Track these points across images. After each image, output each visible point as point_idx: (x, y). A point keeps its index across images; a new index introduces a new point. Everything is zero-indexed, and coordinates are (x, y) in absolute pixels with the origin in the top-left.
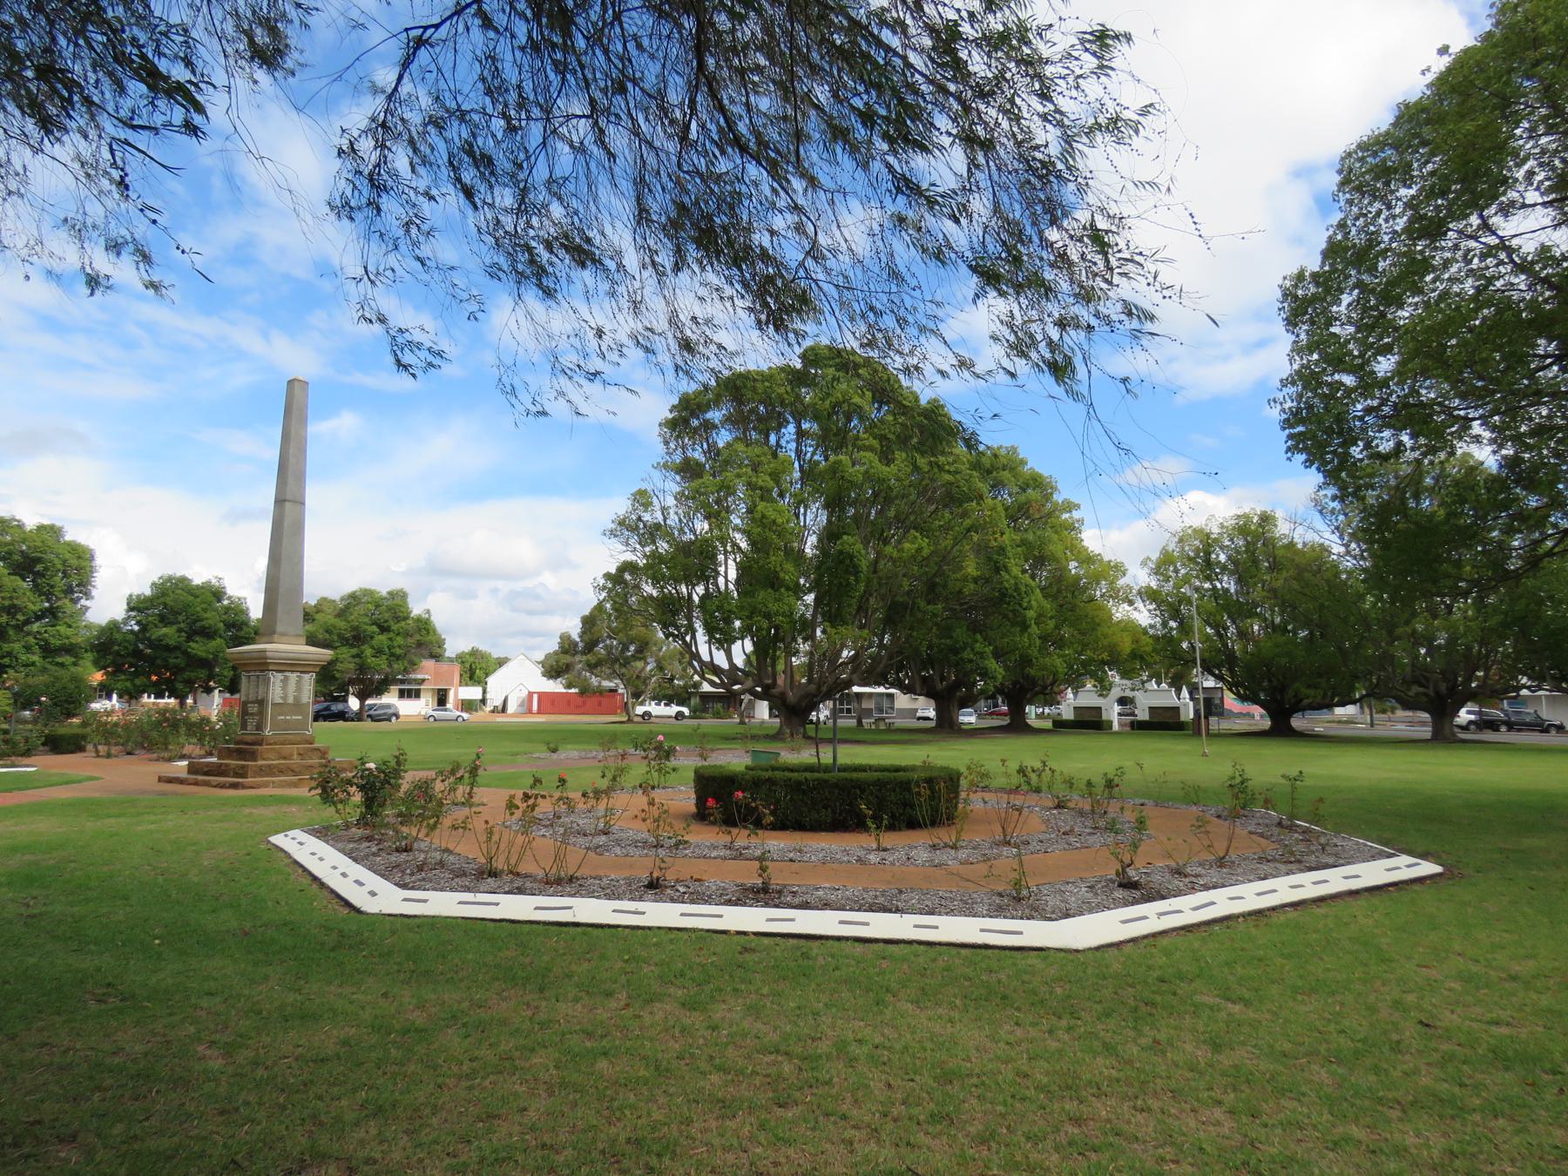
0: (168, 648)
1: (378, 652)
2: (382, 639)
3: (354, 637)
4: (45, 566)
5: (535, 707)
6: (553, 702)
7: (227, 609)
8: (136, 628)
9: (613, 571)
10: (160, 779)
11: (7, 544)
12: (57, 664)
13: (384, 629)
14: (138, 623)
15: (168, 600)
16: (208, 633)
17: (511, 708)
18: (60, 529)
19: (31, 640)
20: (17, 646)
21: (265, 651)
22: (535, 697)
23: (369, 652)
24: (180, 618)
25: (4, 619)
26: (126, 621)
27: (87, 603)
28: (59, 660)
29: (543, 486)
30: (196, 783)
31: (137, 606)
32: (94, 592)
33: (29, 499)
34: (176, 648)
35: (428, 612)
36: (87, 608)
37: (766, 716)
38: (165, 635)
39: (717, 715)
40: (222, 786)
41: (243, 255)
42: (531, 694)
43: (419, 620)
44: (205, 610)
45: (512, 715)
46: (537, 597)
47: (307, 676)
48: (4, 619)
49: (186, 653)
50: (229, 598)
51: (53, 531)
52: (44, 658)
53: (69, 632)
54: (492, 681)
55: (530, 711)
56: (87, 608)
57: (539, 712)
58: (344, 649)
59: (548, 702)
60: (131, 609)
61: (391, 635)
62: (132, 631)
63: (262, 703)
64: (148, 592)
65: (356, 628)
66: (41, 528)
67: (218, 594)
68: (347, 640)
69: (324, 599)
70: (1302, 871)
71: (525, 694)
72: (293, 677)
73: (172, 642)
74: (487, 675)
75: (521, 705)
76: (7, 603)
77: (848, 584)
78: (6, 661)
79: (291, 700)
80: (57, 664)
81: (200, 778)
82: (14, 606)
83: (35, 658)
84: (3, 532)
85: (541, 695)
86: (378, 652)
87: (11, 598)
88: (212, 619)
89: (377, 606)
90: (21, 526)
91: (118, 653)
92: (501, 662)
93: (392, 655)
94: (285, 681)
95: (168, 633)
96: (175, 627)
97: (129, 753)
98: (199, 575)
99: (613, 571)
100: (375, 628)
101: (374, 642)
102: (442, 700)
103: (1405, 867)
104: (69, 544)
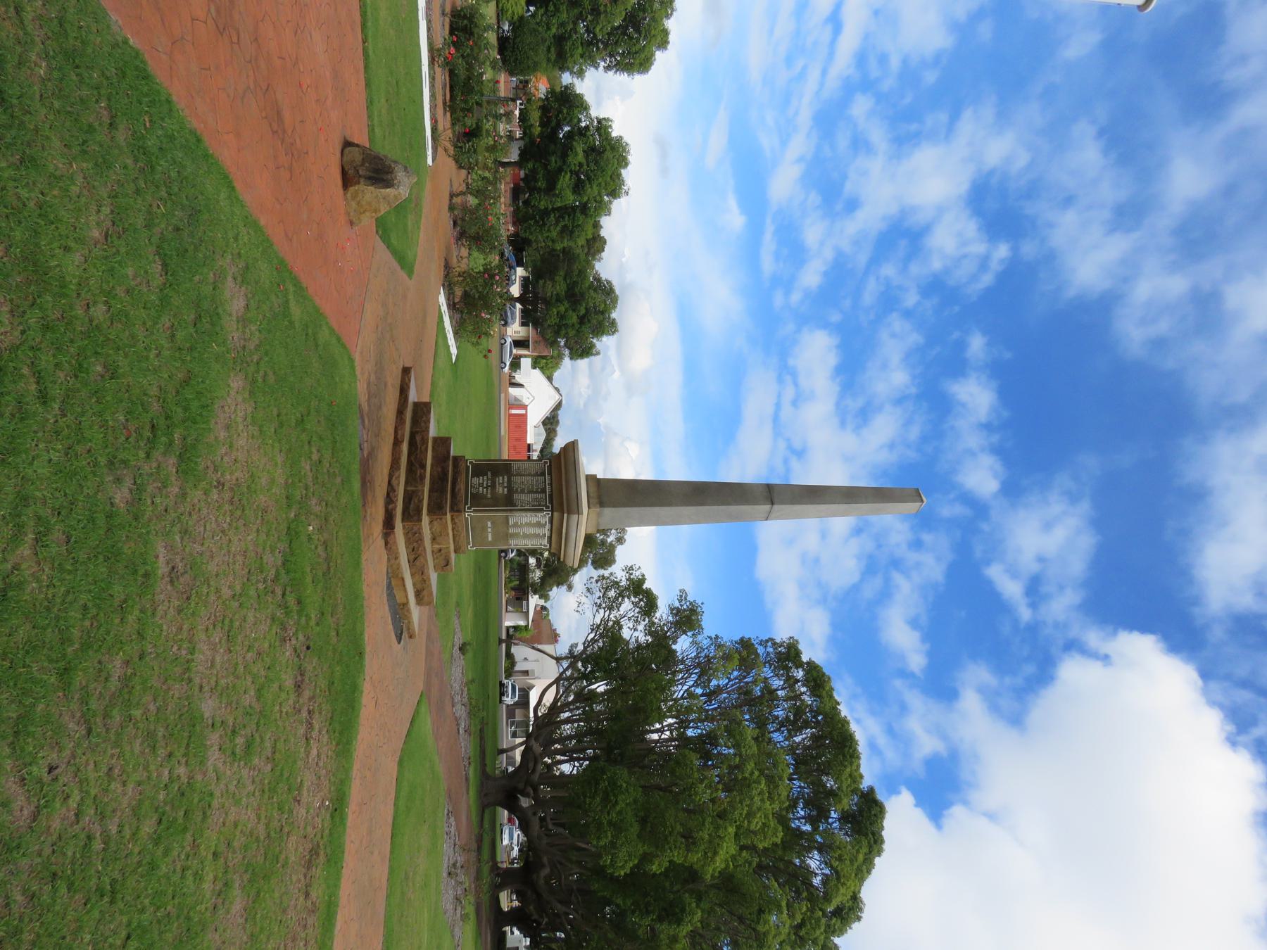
0: (564, 156)
1: (562, 317)
2: (573, 318)
4: (633, 38)
5: (514, 412)
7: (601, 201)
8: (583, 124)
10: (406, 371)
11: (652, 7)
12: (549, 48)
13: (582, 320)
14: (587, 127)
15: (608, 154)
16: (578, 187)
17: (513, 391)
18: (665, 48)
19: (570, 26)
20: (564, 16)
21: (579, 512)
22: (523, 412)
24: (592, 166)
25: (587, 4)
26: (589, 117)
27: (601, 68)
28: (553, 49)
30: (400, 412)
31: (602, 126)
32: (611, 73)
33: (685, 22)
34: (564, 162)
35: (598, 353)
36: (597, 68)
37: (507, 624)
38: (576, 155)
39: (509, 580)
41: (860, 144)
43: (592, 346)
44: (599, 185)
45: (507, 393)
46: (603, 369)
47: (545, 541)
48: (587, 4)
49: (560, 170)
50: (610, 202)
51: (663, 44)
52: (554, 36)
53: (577, 56)
55: (512, 407)
56: (597, 68)
60: (599, 121)
61: (577, 326)
62: (580, 121)
64: (614, 134)
65: (582, 295)
66: (666, 33)
67: (615, 193)
69: (605, 242)
71: (526, 402)
72: (546, 531)
73: (570, 159)
74: (542, 369)
75: (516, 399)
76: (602, 9)
77: (648, 912)
78: (551, 8)
80: (549, 48)
82: (599, 14)
83: (554, 30)
84: (662, 3)
85: (524, 417)
86: (562, 317)
87: (605, 11)
88: (591, 191)
90: (668, 16)
91: (560, 112)
92: (550, 379)
94: (539, 525)
95: (578, 155)
96: (584, 161)
97: (455, 223)
98: (631, 175)
100: (583, 311)
102: (519, 344)
103: (454, 351)
104: (653, 55)
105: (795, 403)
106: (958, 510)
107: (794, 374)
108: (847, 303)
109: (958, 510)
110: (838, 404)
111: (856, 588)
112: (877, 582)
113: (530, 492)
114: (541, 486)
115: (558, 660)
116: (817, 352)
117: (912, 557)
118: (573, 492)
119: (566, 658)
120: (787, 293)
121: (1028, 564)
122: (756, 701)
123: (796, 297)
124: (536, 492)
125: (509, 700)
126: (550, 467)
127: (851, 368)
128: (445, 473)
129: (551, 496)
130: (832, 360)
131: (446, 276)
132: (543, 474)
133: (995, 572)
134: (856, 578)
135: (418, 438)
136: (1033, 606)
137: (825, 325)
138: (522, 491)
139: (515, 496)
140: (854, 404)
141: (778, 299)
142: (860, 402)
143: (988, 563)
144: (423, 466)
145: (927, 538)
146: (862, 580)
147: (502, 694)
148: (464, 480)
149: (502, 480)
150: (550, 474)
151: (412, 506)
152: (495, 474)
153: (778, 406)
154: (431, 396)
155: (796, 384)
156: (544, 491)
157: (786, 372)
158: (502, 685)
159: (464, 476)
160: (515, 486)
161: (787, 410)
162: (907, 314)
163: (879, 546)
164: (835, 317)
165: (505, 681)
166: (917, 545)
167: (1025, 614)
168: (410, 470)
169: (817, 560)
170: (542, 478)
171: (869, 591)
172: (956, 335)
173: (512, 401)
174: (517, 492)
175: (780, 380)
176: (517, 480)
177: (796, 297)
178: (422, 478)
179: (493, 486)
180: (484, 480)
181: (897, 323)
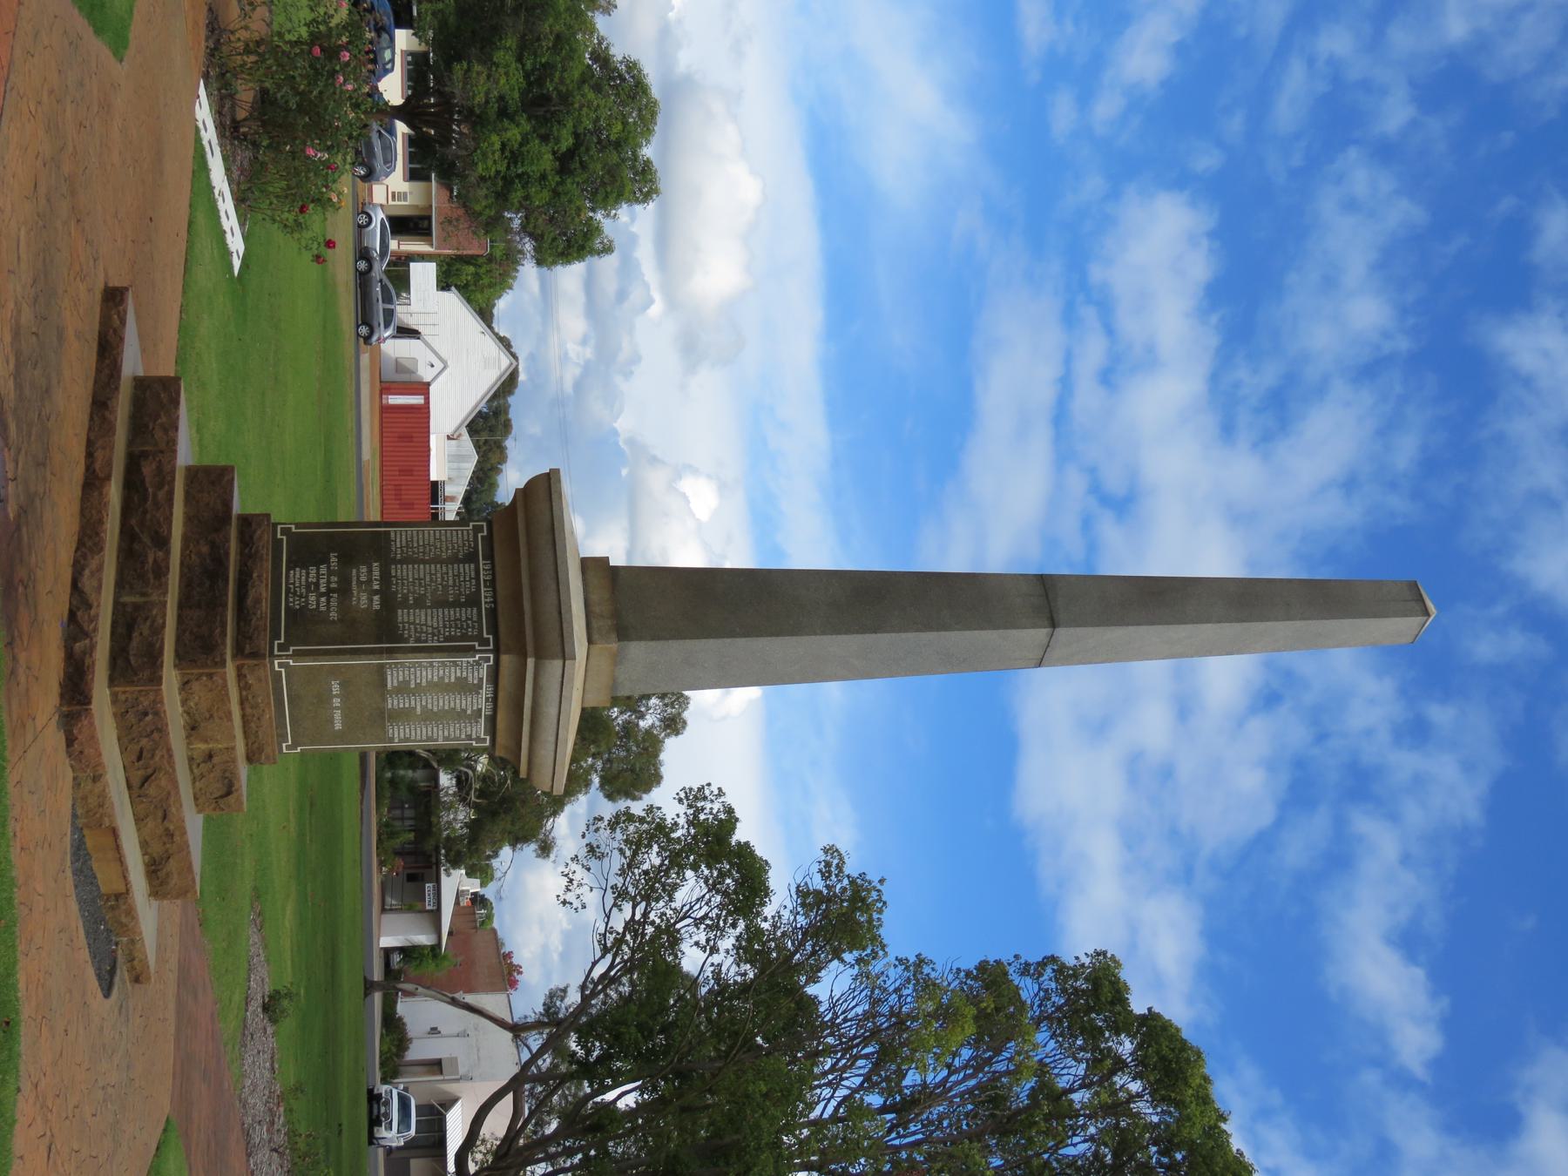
3: (544, 100)
6: (406, 438)
9: (740, 835)
10: (113, 297)
13: (565, 162)
22: (417, 400)
23: (514, 134)
29: (845, 291)
30: (100, 404)
37: (386, 941)
40: (93, 482)
42: (423, 388)
43: (592, 230)
47: (481, 728)
54: (452, 299)
55: (387, 388)
57: (386, 410)
58: (517, 78)
59: (407, 430)
61: (554, 179)
63: (384, 633)
65: (565, 98)
68: (540, 82)
70: (178, 793)
71: (425, 374)
72: (482, 701)
75: (399, 366)
79: (393, 703)
81: (114, 493)
85: (423, 412)
89: (618, 145)
93: (508, 182)
94: (463, 687)
99: (740, 835)
100: (567, 142)
101: (535, 143)
102: (402, 225)
105: (1108, 377)
106: (1517, 644)
107: (1105, 306)
108: (1235, 125)
109: (1517, 644)
110: (1214, 378)
111: (1264, 841)
113: (441, 603)
114: (468, 589)
115: (518, 1030)
116: (1161, 249)
117: (1405, 762)
120: (1085, 99)
123: (1106, 108)
124: (456, 604)
125: (392, 1136)
126: (489, 540)
127: (1244, 294)
128: (219, 561)
129: (493, 613)
130: (1200, 268)
131: (212, 53)
132: (471, 557)
134: (1266, 816)
137: (1181, 181)
138: (419, 603)
139: (402, 615)
140: (1256, 380)
141: (1063, 114)
142: (1270, 375)
144: (162, 542)
145: (1441, 715)
146: (1279, 823)
147: (374, 1122)
149: (366, 573)
150: (490, 556)
153: (1066, 384)
155: (1110, 331)
156: (473, 601)
157: (1083, 298)
158: (374, 1098)
159: (269, 565)
160: (400, 590)
161: (1087, 396)
162: (1384, 152)
163: (1321, 738)
164: (1206, 160)
165: (383, 1089)
166: (1416, 732)
169: (1167, 773)
170: (469, 568)
171: (1297, 850)
172: (1507, 204)
173: (390, 375)
174: (404, 604)
175: (1069, 318)
177: (1106, 108)
178: (161, 571)
179: (344, 590)
180: (322, 576)
181: (1360, 175)
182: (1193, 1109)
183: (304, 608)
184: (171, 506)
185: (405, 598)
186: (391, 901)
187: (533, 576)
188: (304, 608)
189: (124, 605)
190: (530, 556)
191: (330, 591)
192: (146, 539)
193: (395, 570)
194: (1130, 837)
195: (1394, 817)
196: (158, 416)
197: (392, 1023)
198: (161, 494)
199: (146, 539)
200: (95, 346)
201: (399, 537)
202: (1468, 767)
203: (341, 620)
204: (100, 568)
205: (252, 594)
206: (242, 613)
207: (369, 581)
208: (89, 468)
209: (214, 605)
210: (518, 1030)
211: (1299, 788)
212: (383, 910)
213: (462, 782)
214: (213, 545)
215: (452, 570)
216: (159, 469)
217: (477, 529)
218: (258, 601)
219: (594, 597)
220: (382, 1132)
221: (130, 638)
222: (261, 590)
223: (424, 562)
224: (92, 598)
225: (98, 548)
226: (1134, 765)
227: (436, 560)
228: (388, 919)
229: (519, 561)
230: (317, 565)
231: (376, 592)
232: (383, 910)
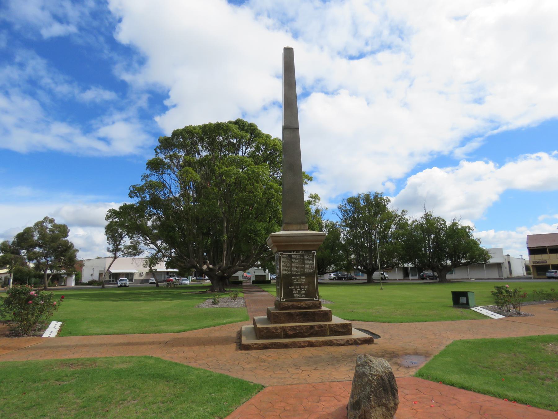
9: (117, 209)
37: (73, 285)
111: (43, 105)
112: (40, 92)
113: (303, 262)
114: (299, 257)
115: (115, 258)
117: (29, 70)
118: (319, 238)
119: (115, 254)
121: (45, 16)
122: (152, 168)
124: (303, 259)
125: (128, 283)
126: (284, 252)
128: (301, 314)
129: (306, 251)
131: (7, 336)
132: (290, 256)
133: (46, 33)
134: (36, 103)
135: (291, 333)
136: (68, 23)
138: (303, 268)
139: (307, 271)
143: (40, 36)
144: (312, 327)
145: (18, 59)
146: (38, 100)
147: (125, 286)
148: (299, 303)
149: (295, 280)
150: (290, 251)
151: (341, 330)
152: (292, 284)
154: (526, 315)
156: (303, 255)
158: (121, 286)
159: (295, 303)
160: (300, 272)
163: (19, 86)
165: (119, 284)
166: (22, 65)
167: (72, 29)
168: (316, 334)
169: (21, 120)
170: (293, 256)
171: (47, 99)
174: (304, 271)
176: (294, 271)
178: (320, 326)
179: (300, 285)
180: (296, 290)
182: (196, 131)
183: (305, 294)
184: (300, 326)
185: (302, 271)
186: (63, 284)
187: (301, 242)
188: (305, 294)
189: (330, 334)
190: (291, 242)
191: (300, 288)
192: (312, 331)
193: (294, 272)
194: (36, 131)
195: (42, 77)
196: (273, 332)
197: (90, 283)
198: (298, 328)
199: (312, 331)
200: (264, 350)
201: (284, 272)
202: (33, 58)
203: (308, 285)
204: (336, 340)
205: (304, 306)
206: (310, 307)
207: (297, 279)
208: (308, 346)
209: (314, 314)
210: (115, 258)
211: (32, 95)
212: (65, 285)
213: (51, 268)
214: (297, 316)
215: (293, 260)
216: (290, 330)
217: (281, 254)
218: (306, 304)
219: (295, 228)
220: (128, 284)
221: (340, 331)
222: (303, 304)
223: (291, 267)
224: (345, 340)
225: (299, 342)
226: (19, 127)
227: (291, 264)
228: (67, 285)
229: (291, 245)
230: (293, 291)
231: (300, 277)
232: (65, 285)
